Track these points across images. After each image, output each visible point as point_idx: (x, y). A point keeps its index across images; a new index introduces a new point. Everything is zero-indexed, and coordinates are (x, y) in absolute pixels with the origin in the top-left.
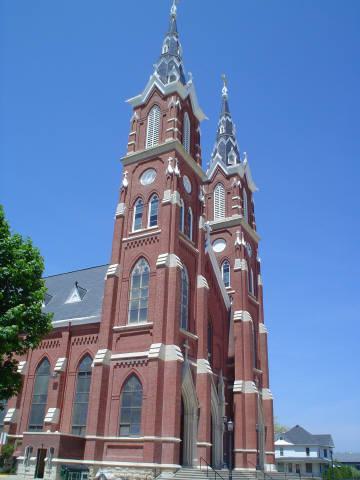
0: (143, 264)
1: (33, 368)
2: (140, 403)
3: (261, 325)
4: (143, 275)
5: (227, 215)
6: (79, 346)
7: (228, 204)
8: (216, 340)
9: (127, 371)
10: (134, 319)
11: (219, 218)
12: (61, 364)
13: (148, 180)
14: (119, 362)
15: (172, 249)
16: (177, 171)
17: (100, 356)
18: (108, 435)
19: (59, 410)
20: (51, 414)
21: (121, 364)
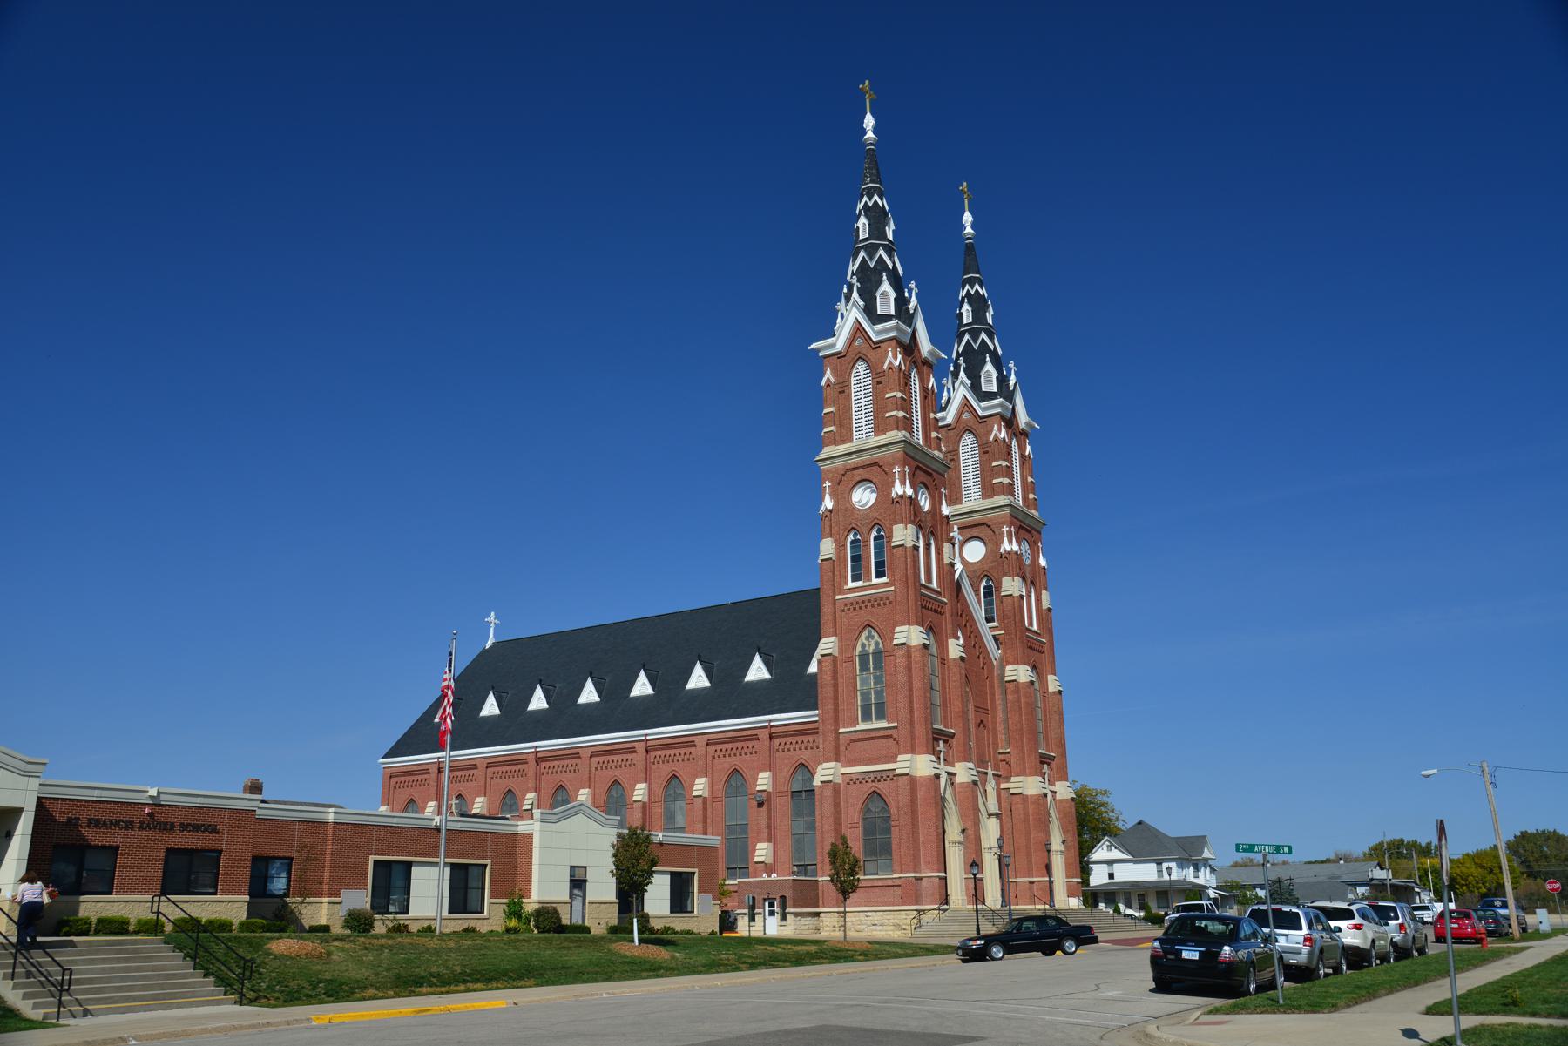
0: (870, 637)
1: (720, 788)
2: (888, 831)
3: (390, 907)
4: (873, 653)
5: (985, 496)
6: (499, 781)
7: (987, 473)
8: (910, 952)
9: (867, 788)
10: (867, 717)
11: (972, 499)
12: (641, 792)
13: (863, 497)
14: (872, 776)
15: (913, 619)
16: (909, 492)
17: (826, 772)
18: (824, 907)
19: (771, 845)
20: (762, 852)
21: (852, 780)
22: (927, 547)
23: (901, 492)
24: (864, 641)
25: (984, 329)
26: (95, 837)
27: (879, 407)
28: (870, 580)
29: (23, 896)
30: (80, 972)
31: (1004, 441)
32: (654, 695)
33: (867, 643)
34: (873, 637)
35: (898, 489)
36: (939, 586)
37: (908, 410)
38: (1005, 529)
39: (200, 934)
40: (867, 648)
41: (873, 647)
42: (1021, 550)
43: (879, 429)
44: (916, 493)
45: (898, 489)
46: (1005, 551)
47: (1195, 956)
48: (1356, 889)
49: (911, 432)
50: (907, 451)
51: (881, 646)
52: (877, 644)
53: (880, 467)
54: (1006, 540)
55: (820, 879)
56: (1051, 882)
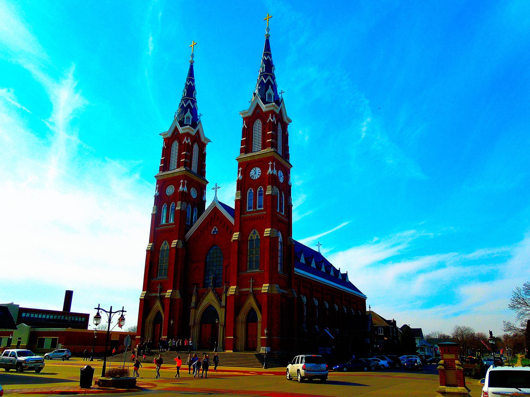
23: (271, 173)
24: (252, 235)
25: (270, 75)
27: (264, 136)
28: (256, 209)
29: (84, 360)
32: (397, 328)
33: (253, 236)
38: (270, 163)
39: (207, 372)
40: (253, 238)
41: (255, 238)
42: (278, 175)
43: (264, 147)
44: (277, 172)
47: (354, 356)
48: (207, 262)
49: (277, 148)
51: (259, 237)
52: (257, 236)
54: (270, 168)
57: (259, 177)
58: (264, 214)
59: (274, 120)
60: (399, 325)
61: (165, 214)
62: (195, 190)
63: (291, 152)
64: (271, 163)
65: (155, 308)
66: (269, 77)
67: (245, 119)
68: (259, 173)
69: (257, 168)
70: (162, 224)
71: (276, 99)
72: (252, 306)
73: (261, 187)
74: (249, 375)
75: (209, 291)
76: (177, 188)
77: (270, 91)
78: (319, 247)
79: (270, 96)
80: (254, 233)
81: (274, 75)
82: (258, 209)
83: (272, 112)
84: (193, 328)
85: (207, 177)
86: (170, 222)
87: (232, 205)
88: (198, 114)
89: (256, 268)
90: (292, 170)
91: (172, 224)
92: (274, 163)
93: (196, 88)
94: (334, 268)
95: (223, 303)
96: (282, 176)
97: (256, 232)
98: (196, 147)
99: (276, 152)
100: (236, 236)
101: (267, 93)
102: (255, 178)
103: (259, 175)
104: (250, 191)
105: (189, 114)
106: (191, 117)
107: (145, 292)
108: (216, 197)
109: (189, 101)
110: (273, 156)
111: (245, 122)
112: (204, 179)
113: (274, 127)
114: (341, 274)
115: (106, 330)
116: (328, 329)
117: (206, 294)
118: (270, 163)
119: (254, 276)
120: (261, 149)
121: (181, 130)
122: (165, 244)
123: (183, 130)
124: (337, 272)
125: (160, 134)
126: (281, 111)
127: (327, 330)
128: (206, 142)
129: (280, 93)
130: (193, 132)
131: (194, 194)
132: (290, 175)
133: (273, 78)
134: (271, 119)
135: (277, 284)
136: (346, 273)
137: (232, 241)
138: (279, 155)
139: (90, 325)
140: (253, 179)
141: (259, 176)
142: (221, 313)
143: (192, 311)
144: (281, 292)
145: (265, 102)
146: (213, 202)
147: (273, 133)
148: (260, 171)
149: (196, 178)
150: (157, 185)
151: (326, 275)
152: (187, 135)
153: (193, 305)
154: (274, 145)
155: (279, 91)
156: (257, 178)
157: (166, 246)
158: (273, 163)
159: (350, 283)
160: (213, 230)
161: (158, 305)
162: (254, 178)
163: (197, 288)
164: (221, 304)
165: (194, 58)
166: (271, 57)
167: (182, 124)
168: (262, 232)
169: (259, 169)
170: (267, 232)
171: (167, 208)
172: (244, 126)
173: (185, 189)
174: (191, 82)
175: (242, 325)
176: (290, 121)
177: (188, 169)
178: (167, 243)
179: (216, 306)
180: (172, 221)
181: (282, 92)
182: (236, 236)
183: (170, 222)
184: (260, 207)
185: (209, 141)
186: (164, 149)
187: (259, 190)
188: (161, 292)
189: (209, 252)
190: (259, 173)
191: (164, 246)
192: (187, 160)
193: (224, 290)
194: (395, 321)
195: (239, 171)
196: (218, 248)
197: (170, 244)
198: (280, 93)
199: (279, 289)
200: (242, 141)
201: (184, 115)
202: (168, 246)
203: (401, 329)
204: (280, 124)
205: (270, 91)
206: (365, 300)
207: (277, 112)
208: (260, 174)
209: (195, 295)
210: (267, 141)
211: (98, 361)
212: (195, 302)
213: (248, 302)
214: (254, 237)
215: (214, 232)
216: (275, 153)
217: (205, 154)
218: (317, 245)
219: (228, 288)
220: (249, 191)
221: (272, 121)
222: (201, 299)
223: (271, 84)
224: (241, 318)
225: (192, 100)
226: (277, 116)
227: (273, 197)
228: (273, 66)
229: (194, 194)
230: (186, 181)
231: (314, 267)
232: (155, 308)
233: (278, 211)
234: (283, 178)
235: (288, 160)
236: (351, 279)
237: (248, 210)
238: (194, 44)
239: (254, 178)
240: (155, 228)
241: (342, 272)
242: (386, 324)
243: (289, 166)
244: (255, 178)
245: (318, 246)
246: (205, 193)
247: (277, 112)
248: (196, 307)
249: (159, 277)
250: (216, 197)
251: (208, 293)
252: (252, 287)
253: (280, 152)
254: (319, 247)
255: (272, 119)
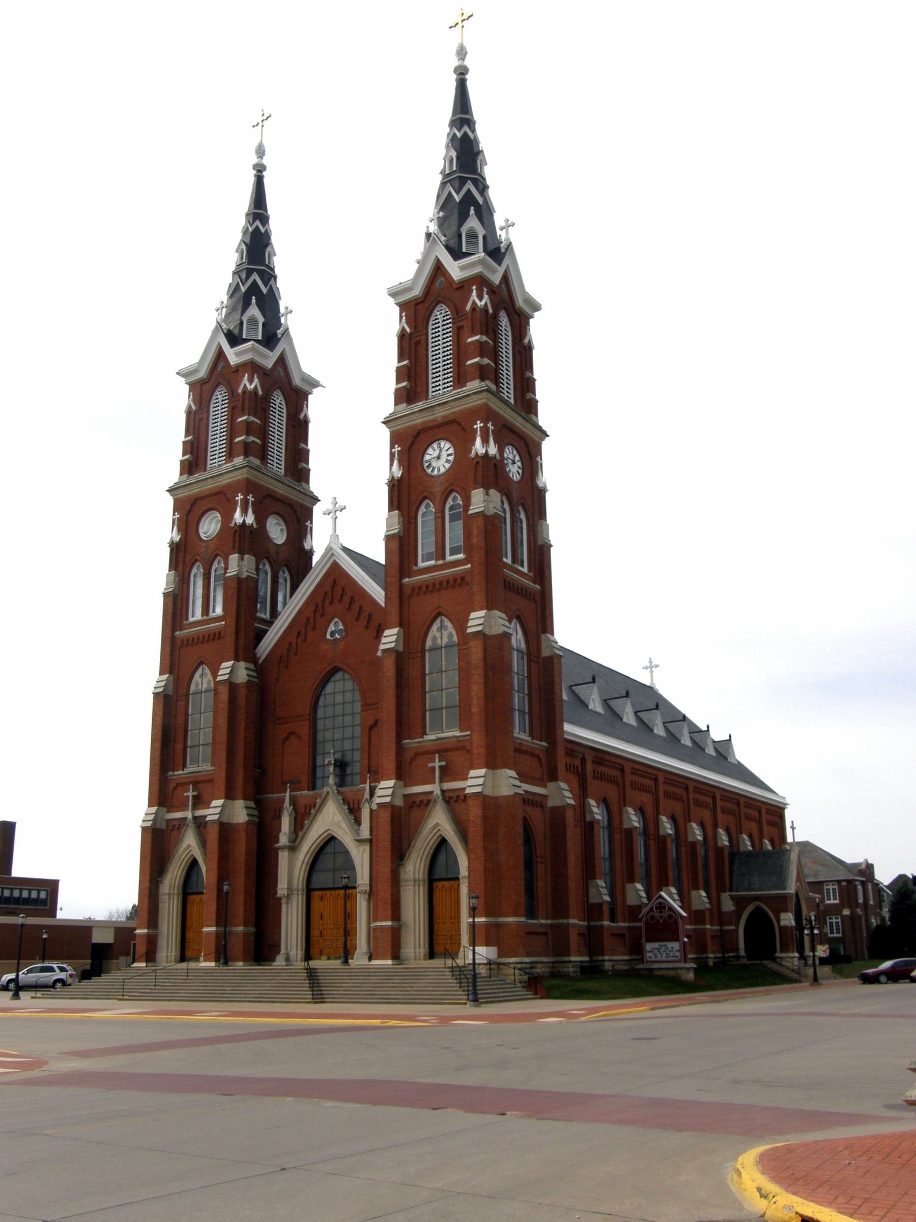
16: (493, 450)
22: (515, 520)
25: (471, 179)
26: (471, 905)
27: (460, 353)
28: (444, 558)
30: (307, 987)
31: (487, 311)
32: (877, 886)
34: (446, 628)
35: (478, 447)
36: (530, 569)
37: (495, 355)
38: (479, 425)
40: (439, 641)
45: (478, 447)
46: (477, 454)
49: (497, 381)
50: (245, 240)
51: (455, 638)
52: (450, 636)
53: (459, 424)
55: (606, 958)
56: (308, 957)
57: (450, 468)
58: (467, 572)
59: (484, 301)
60: (885, 876)
61: (199, 591)
62: (282, 522)
63: (542, 393)
64: (482, 425)
65: (182, 854)
66: (470, 186)
67: (403, 306)
68: (448, 455)
69: (443, 443)
70: (191, 619)
71: (491, 247)
72: (441, 835)
73: (455, 496)
74: (421, 1026)
75: (325, 797)
76: (227, 516)
77: (473, 222)
78: (652, 672)
79: (472, 236)
80: (442, 628)
81: (484, 179)
82: (449, 558)
83: (481, 281)
84: (287, 903)
85: (316, 485)
86: (212, 615)
87: (378, 554)
88: (282, 310)
89: (450, 727)
90: (546, 445)
91: (218, 619)
92: (490, 425)
93: (274, 239)
94: (691, 724)
95: (365, 832)
96: (518, 461)
97: (447, 623)
98: (278, 400)
99: (497, 395)
100: (390, 638)
101: (464, 230)
102: (439, 470)
103: (447, 461)
104: (425, 514)
105: (254, 311)
106: (261, 320)
107: (154, 809)
108: (335, 536)
109: (255, 277)
110: (486, 405)
111: (406, 316)
112: (304, 489)
113: (489, 325)
114: (714, 742)
115: (446, 960)
116: (673, 890)
117: (319, 808)
118: (479, 425)
119: (444, 750)
120: (451, 388)
121: (233, 356)
122: (202, 676)
123: (238, 354)
124: (699, 735)
125: (178, 373)
126: (506, 278)
127: (670, 894)
128: (305, 387)
129: (502, 229)
130: (269, 360)
131: (277, 532)
132: (541, 459)
133: (483, 187)
134: (478, 300)
135: (510, 768)
136: (728, 738)
137: (379, 654)
138: (506, 403)
139: (61, 909)
140: (433, 474)
141: (448, 466)
142: (361, 858)
143: (283, 858)
144: (524, 791)
145: (456, 253)
146: (329, 549)
147: (484, 338)
148: (451, 451)
149: (281, 490)
150: (174, 515)
151: (671, 744)
152: (252, 367)
153: (284, 839)
154: (491, 374)
155: (499, 221)
156: (442, 470)
157: (205, 680)
158: (486, 425)
159: (739, 763)
160: (332, 628)
161: (189, 844)
162: (436, 472)
163: (292, 793)
164: (358, 834)
165: (264, 158)
166: (473, 131)
167: (234, 339)
168: (461, 624)
169: (448, 445)
170: (477, 620)
171: (204, 575)
172: (403, 327)
173: (250, 519)
174: (258, 223)
175: (417, 887)
176: (536, 307)
177: (257, 462)
178: (207, 671)
179: (346, 837)
180: (219, 610)
181: (509, 225)
182: (390, 638)
183: (212, 615)
184: (454, 551)
185: (315, 384)
186: (189, 413)
187: (450, 502)
188: (195, 806)
189: (321, 692)
190: (448, 455)
191: (202, 680)
192: (251, 439)
193: (367, 795)
194: (872, 866)
195: (392, 456)
196: (347, 676)
197: (215, 675)
198: (502, 229)
199: (517, 783)
200: (398, 370)
201: (243, 313)
202: (209, 682)
203: (889, 887)
204: (505, 315)
205: (473, 222)
206: (783, 809)
207: (496, 279)
208: (451, 458)
209: (288, 811)
210: (469, 362)
211: (33, 998)
212: (290, 833)
213: (431, 823)
214: (441, 638)
215: (332, 634)
216: (490, 396)
217: (305, 423)
218: (646, 668)
219: (375, 787)
220: (422, 509)
221: (479, 305)
222: (306, 822)
223: (475, 203)
224: (413, 868)
225: (261, 274)
226: (493, 291)
227: (491, 523)
228: (480, 152)
229: (277, 532)
230: (251, 498)
231: (660, 733)
232: (182, 854)
233: (508, 560)
234: (519, 467)
235: (533, 417)
236: (742, 754)
237: (421, 564)
238: (265, 117)
239: (436, 472)
240: (174, 630)
241: (717, 735)
242: (843, 875)
243: (539, 433)
244: (439, 470)
245: (649, 669)
246: (311, 528)
247: (496, 279)
248: (293, 848)
249: (190, 768)
250: (335, 536)
251: (323, 804)
252: (441, 781)
253: (509, 393)
254: (652, 672)
255: (481, 299)
